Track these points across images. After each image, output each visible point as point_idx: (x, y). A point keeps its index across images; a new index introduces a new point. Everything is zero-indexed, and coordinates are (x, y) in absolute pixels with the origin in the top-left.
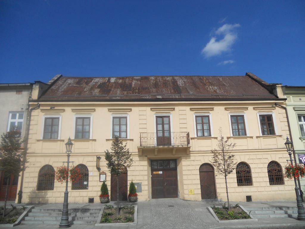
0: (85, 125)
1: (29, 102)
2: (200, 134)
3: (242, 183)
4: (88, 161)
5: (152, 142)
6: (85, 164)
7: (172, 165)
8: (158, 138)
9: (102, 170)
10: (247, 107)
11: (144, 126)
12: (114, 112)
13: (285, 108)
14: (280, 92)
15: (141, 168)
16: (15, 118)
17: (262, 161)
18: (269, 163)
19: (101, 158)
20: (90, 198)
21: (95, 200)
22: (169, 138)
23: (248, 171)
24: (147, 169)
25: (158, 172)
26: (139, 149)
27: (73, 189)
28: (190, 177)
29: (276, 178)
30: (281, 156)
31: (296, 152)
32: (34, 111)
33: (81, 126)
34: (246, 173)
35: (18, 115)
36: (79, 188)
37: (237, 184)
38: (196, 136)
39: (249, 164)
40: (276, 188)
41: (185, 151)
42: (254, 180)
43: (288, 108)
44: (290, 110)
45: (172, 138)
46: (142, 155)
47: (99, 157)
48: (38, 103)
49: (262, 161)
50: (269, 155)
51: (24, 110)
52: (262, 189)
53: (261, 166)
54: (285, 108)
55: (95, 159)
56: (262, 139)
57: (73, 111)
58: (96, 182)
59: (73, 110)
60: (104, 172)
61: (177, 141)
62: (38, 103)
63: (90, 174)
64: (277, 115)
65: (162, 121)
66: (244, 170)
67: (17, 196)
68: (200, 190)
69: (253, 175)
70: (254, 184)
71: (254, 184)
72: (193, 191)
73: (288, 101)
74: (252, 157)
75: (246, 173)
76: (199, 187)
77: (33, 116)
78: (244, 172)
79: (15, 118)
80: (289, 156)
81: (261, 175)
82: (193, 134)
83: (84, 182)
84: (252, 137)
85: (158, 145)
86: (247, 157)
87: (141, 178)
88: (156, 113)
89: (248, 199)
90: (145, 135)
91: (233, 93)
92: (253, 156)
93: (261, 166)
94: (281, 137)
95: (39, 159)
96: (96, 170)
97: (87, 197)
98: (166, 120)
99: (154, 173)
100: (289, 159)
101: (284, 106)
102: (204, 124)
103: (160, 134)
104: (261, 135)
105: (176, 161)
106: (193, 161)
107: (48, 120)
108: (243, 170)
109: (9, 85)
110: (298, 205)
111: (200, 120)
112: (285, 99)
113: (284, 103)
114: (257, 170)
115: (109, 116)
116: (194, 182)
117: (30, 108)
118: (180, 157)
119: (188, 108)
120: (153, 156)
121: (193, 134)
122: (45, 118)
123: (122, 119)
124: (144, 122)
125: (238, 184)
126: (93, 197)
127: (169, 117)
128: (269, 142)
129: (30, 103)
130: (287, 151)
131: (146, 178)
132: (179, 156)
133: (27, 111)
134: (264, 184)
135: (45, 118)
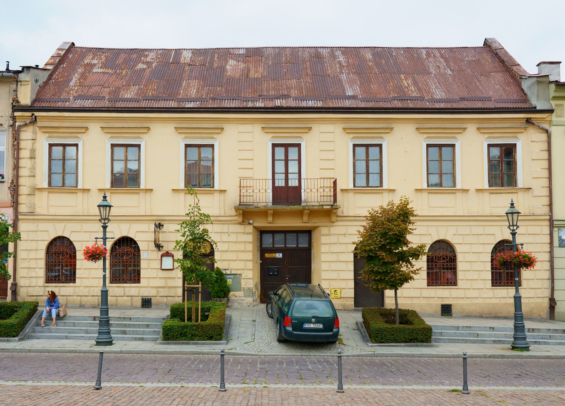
0: (115, 160)
1: (13, 112)
2: (361, 181)
3: (436, 280)
4: (72, 232)
6: (132, 237)
8: (275, 189)
9: (165, 249)
10: (309, 126)
11: (249, 164)
13: (547, 131)
15: (241, 247)
17: (482, 239)
18: (496, 245)
19: (163, 226)
20: (144, 298)
21: (153, 301)
22: (298, 190)
23: (450, 258)
24: (251, 249)
25: (274, 255)
26: (237, 209)
27: (47, 283)
28: (334, 266)
29: (507, 273)
31: (555, 223)
32: (25, 131)
33: (128, 159)
34: (447, 262)
36: (135, 280)
37: (490, 282)
38: (351, 186)
39: (455, 245)
42: (143, 274)
45: (302, 191)
46: (243, 221)
47: (160, 224)
48: (33, 114)
49: (482, 239)
50: (499, 227)
52: (475, 294)
53: (480, 249)
55: (152, 227)
56: (487, 195)
57: (179, 131)
58: (155, 271)
59: (344, 129)
60: (170, 252)
62: (33, 114)
63: (143, 255)
66: (444, 257)
67: (9, 292)
68: (353, 291)
71: (459, 283)
72: (338, 291)
73: (557, 116)
75: (447, 262)
77: (24, 140)
78: (444, 259)
80: (102, 229)
81: (476, 267)
82: (346, 182)
84: (466, 191)
86: (452, 230)
87: (240, 265)
88: (271, 138)
89: (445, 310)
90: (249, 183)
92: (464, 229)
93: (480, 249)
95: (42, 226)
96: (155, 249)
97: (138, 296)
98: (374, 151)
99: (267, 255)
100: (101, 235)
101: (546, 126)
102: (129, 162)
103: (280, 183)
104: (486, 186)
106: (343, 236)
107: (54, 148)
108: (441, 256)
109: (3, 74)
110: (515, 324)
111: (361, 151)
112: (551, 111)
113: (547, 119)
114: (469, 257)
115: (421, 142)
116: (343, 275)
117: (17, 124)
118: (318, 227)
119: (257, 128)
120: (262, 223)
121: (346, 182)
122: (185, 144)
123: (290, 149)
124: (249, 155)
125: (492, 283)
126: (149, 298)
127: (298, 146)
129: (16, 114)
130: (100, 220)
131: (250, 265)
132: (317, 225)
133: (11, 130)
134: (480, 285)
135: (185, 144)
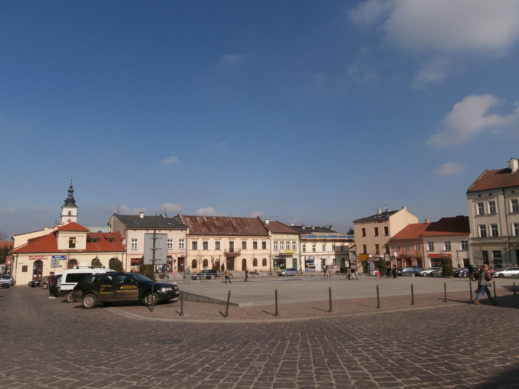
5: (228, 251)
7: (232, 259)
12: (252, 238)
13: (270, 239)
14: (270, 233)
16: (181, 241)
30: (267, 256)
35: (134, 240)
40: (264, 267)
41: (238, 254)
42: (258, 264)
43: (271, 239)
44: (272, 240)
51: (185, 238)
53: (261, 260)
54: (270, 239)
61: (236, 250)
64: (268, 242)
65: (232, 243)
69: (258, 263)
70: (258, 266)
74: (258, 257)
76: (242, 267)
79: (181, 241)
83: (36, 277)
85: (230, 252)
91: (216, 234)
94: (378, 245)
95: (191, 257)
105: (234, 258)
128: (264, 251)
